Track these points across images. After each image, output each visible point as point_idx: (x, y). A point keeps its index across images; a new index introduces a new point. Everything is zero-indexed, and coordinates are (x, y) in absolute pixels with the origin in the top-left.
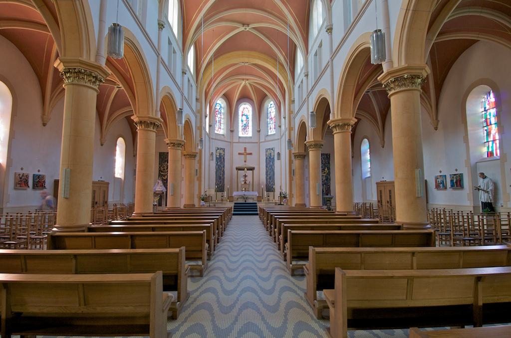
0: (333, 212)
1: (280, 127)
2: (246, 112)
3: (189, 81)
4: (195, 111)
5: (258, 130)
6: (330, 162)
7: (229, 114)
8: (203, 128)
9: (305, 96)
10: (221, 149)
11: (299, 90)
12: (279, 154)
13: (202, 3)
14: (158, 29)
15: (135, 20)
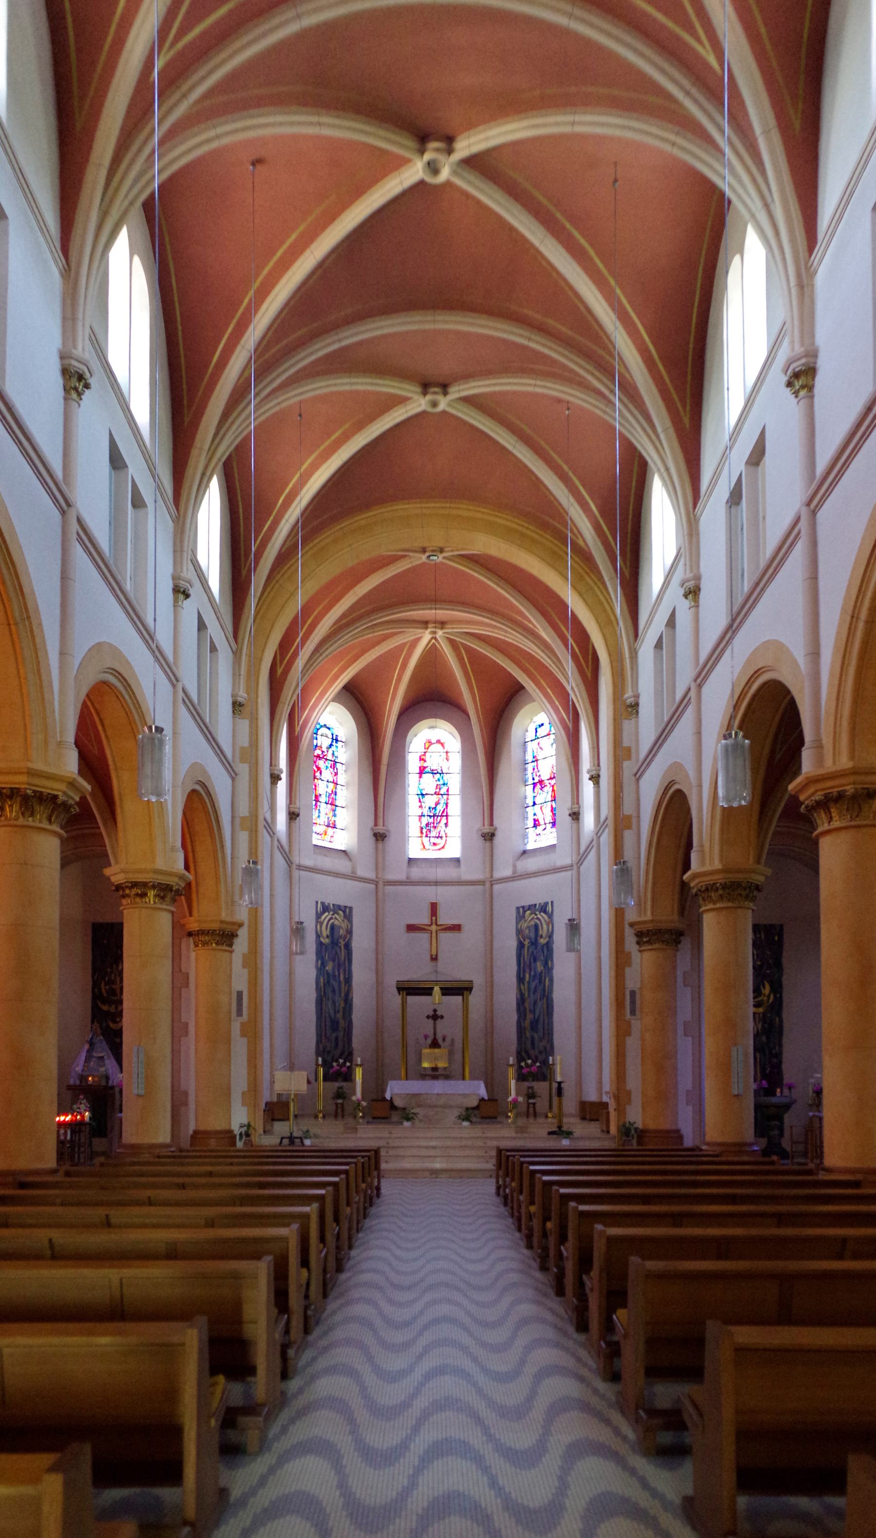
0: (810, 1172)
1: (576, 816)
2: (434, 761)
3: (202, 626)
4: (229, 755)
5: (487, 829)
6: (784, 961)
7: (368, 771)
8: (261, 823)
9: (684, 677)
10: (337, 908)
11: (658, 659)
12: (574, 927)
13: (251, 293)
14: (61, 393)
15: (196, 721)
